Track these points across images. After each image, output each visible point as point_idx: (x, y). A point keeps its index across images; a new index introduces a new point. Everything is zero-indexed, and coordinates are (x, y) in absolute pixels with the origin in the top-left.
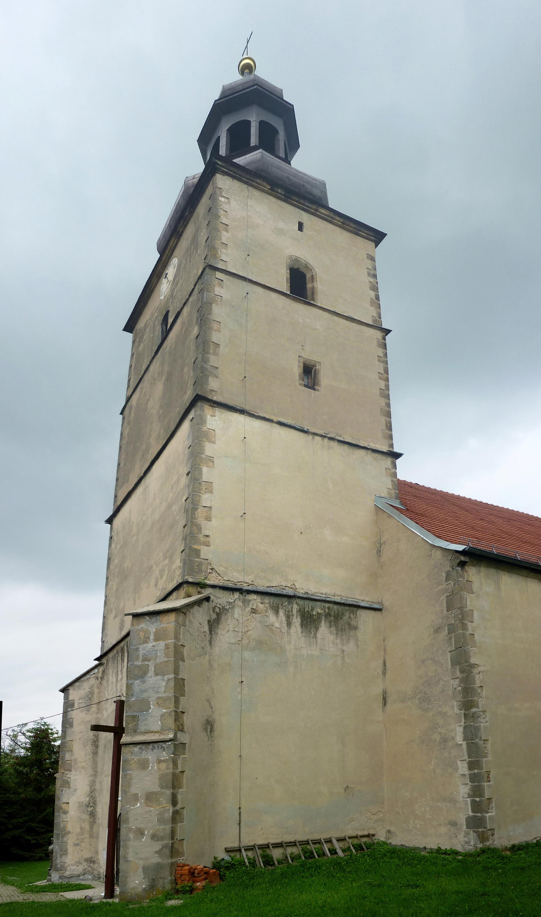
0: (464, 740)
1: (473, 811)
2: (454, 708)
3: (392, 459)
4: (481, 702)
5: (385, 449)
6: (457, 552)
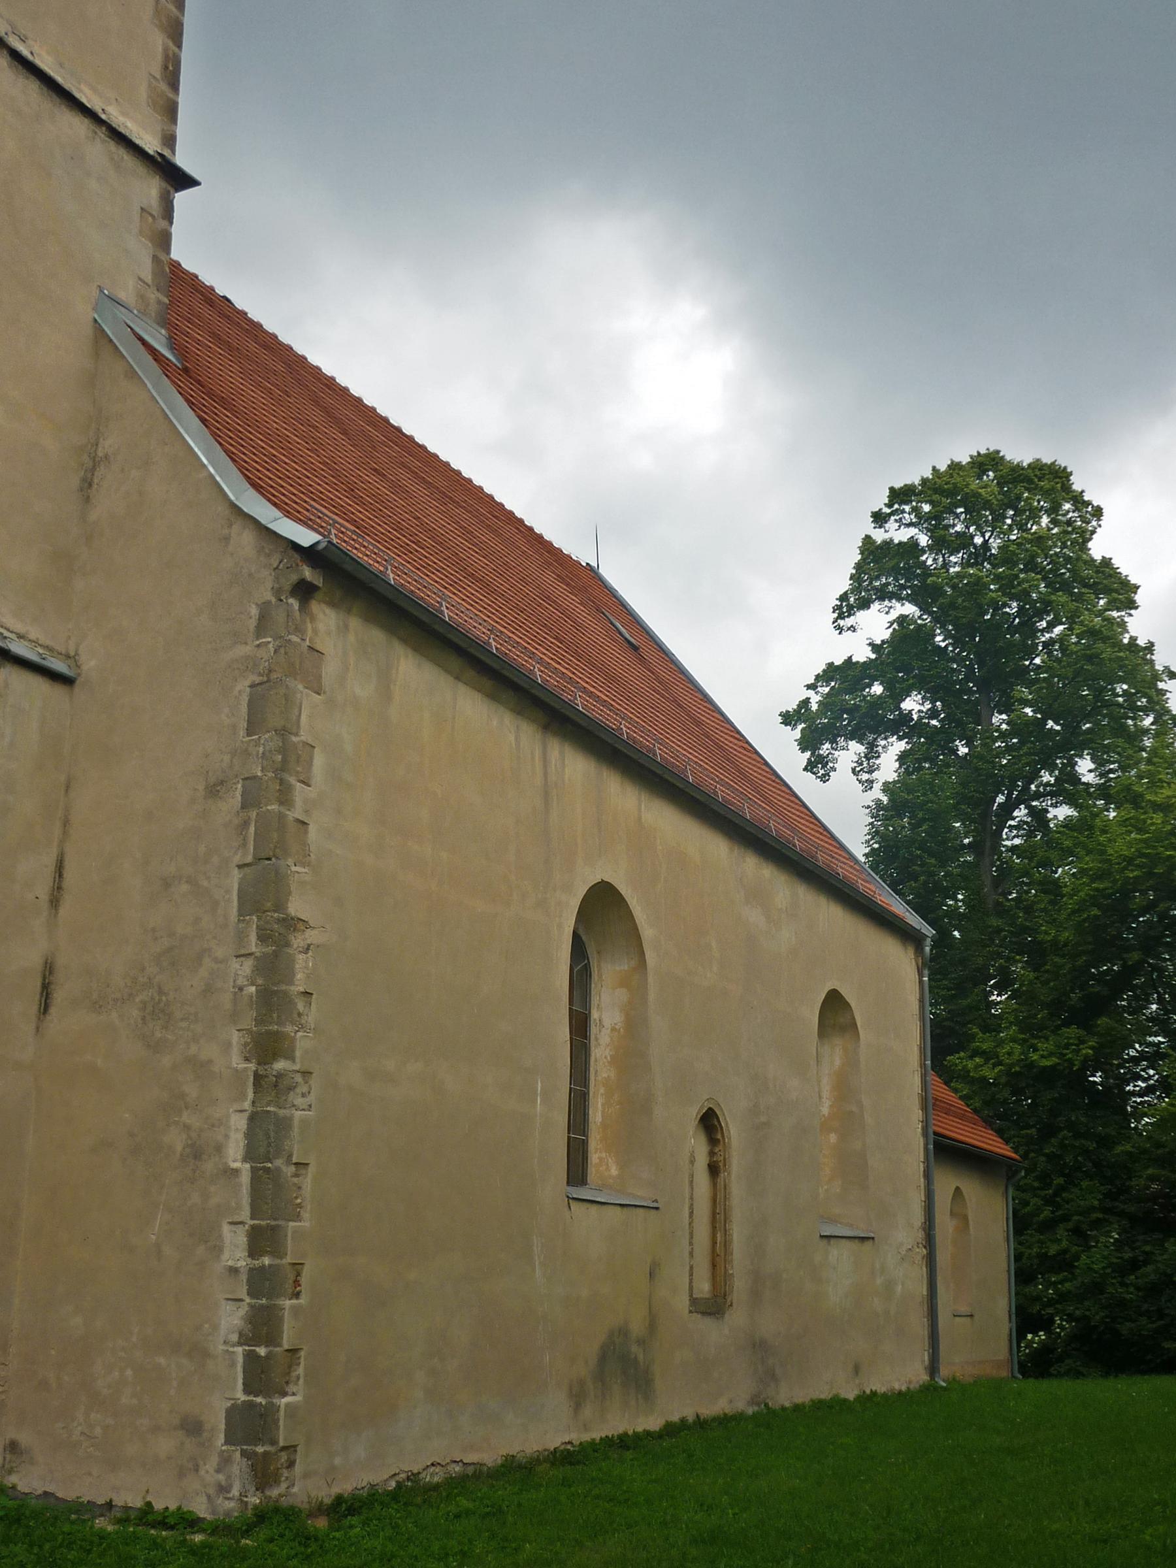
0: (245, 1160)
1: (247, 1390)
2: (231, 1055)
3: (164, 185)
4: (303, 1043)
5: (151, 144)
6: (295, 547)
